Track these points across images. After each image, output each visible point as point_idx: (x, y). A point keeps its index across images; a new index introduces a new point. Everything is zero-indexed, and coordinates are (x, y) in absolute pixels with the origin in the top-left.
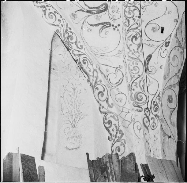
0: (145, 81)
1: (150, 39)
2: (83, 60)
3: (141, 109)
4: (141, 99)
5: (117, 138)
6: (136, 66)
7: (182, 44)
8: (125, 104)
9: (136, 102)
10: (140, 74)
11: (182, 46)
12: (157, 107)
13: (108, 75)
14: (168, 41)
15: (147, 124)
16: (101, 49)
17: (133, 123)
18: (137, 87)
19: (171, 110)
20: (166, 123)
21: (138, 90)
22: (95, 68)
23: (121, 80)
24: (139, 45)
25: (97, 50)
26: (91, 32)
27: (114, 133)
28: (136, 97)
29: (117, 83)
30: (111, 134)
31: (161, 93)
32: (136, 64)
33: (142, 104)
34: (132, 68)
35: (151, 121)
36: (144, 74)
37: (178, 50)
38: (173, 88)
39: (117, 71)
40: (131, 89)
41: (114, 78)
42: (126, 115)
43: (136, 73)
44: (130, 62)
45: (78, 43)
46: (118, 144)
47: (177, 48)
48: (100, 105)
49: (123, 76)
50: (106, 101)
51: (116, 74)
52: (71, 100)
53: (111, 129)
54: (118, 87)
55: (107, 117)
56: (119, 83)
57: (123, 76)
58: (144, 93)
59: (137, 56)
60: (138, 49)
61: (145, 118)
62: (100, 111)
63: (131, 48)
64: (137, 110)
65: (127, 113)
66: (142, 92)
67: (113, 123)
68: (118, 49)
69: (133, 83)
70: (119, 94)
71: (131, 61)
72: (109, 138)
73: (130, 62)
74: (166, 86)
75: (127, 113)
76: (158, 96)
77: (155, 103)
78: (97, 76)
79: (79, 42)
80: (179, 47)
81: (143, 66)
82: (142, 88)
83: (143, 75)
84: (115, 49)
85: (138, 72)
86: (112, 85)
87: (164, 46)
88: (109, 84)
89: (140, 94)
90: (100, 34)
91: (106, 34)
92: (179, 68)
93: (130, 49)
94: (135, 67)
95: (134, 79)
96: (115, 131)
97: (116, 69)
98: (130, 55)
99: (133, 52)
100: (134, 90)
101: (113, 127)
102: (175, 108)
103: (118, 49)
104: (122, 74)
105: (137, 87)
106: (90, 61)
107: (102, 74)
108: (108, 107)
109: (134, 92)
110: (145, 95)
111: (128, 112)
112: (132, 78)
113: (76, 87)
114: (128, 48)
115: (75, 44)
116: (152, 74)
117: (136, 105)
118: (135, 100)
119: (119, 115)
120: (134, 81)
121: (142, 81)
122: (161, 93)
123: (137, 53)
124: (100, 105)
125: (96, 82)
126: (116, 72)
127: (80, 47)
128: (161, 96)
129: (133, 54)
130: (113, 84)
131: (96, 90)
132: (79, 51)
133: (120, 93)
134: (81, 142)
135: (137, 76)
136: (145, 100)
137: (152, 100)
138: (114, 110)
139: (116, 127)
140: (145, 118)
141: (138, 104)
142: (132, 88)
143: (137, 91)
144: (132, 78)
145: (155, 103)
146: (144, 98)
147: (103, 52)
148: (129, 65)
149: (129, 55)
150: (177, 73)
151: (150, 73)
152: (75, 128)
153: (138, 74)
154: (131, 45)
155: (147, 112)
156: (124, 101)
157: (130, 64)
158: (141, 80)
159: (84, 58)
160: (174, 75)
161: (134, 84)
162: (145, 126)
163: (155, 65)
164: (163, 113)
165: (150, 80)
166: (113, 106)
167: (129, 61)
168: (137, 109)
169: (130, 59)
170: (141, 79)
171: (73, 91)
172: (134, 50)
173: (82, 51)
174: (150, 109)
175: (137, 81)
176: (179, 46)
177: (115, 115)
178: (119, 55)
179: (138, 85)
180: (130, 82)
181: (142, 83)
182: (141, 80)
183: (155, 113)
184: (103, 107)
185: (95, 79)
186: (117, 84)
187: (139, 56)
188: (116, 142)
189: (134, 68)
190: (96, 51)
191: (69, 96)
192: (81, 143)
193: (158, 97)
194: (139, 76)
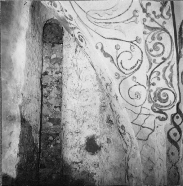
0: (173, 68)
3: (165, 117)
6: (159, 43)
9: (157, 105)
10: (165, 55)
13: (119, 56)
16: (106, 12)
18: (159, 79)
21: (161, 84)
23: (139, 63)
28: (157, 96)
29: (132, 68)
32: (158, 39)
33: (167, 108)
34: (150, 46)
36: (172, 55)
39: (132, 48)
40: (150, 82)
41: (128, 60)
42: (147, 118)
43: (159, 55)
49: (142, 56)
51: (131, 53)
54: (135, 75)
56: (136, 68)
57: (142, 56)
58: (172, 89)
59: (161, 24)
60: (161, 10)
63: (150, 10)
65: (148, 115)
68: (132, 9)
69: (152, 72)
70: (136, 85)
75: (148, 115)
81: (172, 41)
82: (169, 80)
84: (128, 10)
85: (163, 53)
88: (120, 70)
89: (164, 91)
93: (148, 12)
94: (156, 44)
95: (154, 65)
97: (132, 44)
98: (148, 23)
100: (154, 84)
103: (132, 9)
104: (141, 53)
105: (159, 79)
109: (153, 88)
110: (173, 93)
112: (151, 65)
114: (144, 11)
117: (157, 110)
118: (156, 101)
120: (155, 69)
123: (160, 18)
126: (131, 49)
129: (152, 20)
130: (127, 70)
133: (138, 84)
135: (159, 60)
136: (173, 100)
141: (160, 108)
142: (152, 82)
143: (158, 87)
144: (151, 65)
148: (146, 41)
149: (146, 23)
153: (162, 56)
157: (148, 40)
158: (167, 67)
161: (154, 75)
167: (146, 34)
168: (158, 116)
169: (148, 31)
170: (167, 65)
172: (154, 12)
175: (160, 69)
178: (134, 18)
180: (147, 72)
181: (168, 73)
182: (167, 67)
186: (133, 70)
187: (164, 23)
189: (155, 47)
190: (98, 17)
194: (164, 59)
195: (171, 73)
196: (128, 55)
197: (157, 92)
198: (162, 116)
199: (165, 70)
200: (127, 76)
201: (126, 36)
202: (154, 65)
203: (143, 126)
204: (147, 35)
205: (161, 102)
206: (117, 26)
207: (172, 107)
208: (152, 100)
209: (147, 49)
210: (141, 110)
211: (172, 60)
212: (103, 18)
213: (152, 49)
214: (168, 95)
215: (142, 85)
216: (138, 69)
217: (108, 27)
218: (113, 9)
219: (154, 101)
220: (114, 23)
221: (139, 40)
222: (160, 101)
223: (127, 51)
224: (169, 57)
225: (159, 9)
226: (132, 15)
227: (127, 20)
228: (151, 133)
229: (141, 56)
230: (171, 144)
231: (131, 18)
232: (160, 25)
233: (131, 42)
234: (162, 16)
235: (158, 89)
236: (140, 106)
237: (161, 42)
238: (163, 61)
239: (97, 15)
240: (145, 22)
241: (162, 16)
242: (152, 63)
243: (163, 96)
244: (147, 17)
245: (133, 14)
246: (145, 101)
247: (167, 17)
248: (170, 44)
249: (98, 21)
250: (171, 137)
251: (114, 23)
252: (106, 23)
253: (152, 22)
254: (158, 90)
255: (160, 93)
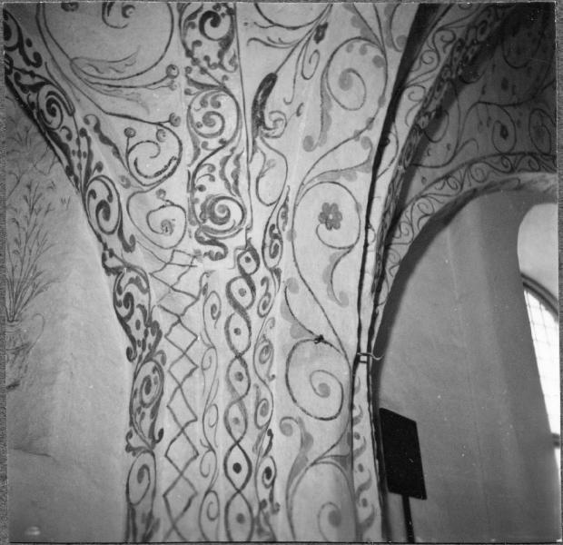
0: (240, 160)
1: (270, 21)
2: (50, 102)
3: (222, 251)
4: (226, 217)
5: (147, 351)
6: (214, 113)
7: (377, 31)
8: (180, 241)
9: (206, 229)
10: (226, 136)
11: (379, 37)
12: (279, 244)
14: (322, 23)
15: (244, 301)
16: (112, 65)
17: (202, 297)
18: (212, 179)
19: (332, 251)
20: (309, 293)
21: (218, 188)
22: (81, 124)
23: (174, 163)
24: (226, 42)
25: (97, 70)
26: (73, 10)
27: (139, 335)
28: (208, 210)
29: (158, 174)
30: (132, 339)
31: (290, 196)
32: (213, 105)
33: (227, 234)
34: (198, 118)
35: (260, 290)
36: (238, 135)
37: (363, 51)
38: (342, 180)
39: (161, 135)
40: (194, 185)
44: (193, 99)
45: (26, 46)
46: (147, 369)
47: (358, 45)
48: (105, 246)
50: (116, 232)
52: (17, 236)
53: (132, 323)
54: (162, 186)
55: (123, 284)
56: (166, 173)
58: (237, 198)
59: (220, 79)
60: (220, 55)
61: (234, 279)
62: (105, 266)
64: (208, 254)
65: (187, 268)
66: (228, 195)
67: (136, 303)
69: (199, 166)
70: (163, 207)
71: (198, 94)
72: (129, 352)
73: (193, 99)
74: (314, 173)
76: (285, 205)
77: (276, 231)
78: (90, 152)
79: (30, 44)
80: (363, 42)
82: (231, 181)
83: (237, 139)
84: (156, 64)
85: (221, 130)
86: (141, 178)
87: (313, 42)
88: (131, 174)
89: (222, 202)
90: (106, 15)
91: (125, 16)
92: (372, 115)
93: (195, 56)
95: (204, 153)
96: (143, 327)
97: (160, 128)
98: (195, 75)
99: (204, 64)
100: (201, 188)
101: (138, 314)
102: (351, 248)
103: (165, 62)
105: (212, 179)
106: (66, 102)
107: (105, 143)
108: (123, 252)
109: (201, 196)
110: (240, 206)
111: (191, 266)
112: (197, 152)
113: (38, 193)
114: (189, 53)
115: (17, 50)
116: (275, 137)
117: (207, 239)
118: (204, 221)
119: (151, 274)
121: (231, 161)
122: (292, 197)
124: (105, 246)
125: (88, 173)
127: (33, 60)
128: (290, 205)
129: (203, 71)
130: (146, 177)
131: (91, 199)
132: (32, 74)
133: (168, 203)
134: (26, 366)
135: (214, 143)
137: (268, 223)
138: (138, 257)
139: (145, 313)
140: (234, 279)
141: (212, 235)
142: (198, 184)
144: (197, 152)
145: (276, 231)
146: (236, 214)
147: (118, 76)
148: (190, 107)
150: (361, 132)
151: (267, 136)
152: (15, 323)
153: (219, 138)
154: (197, 43)
155: (248, 260)
156: (178, 231)
157: (193, 106)
158: (228, 157)
159: (50, 97)
160: (351, 135)
161: (204, 170)
162: (236, 305)
163: (285, 109)
164: (295, 260)
165: (268, 158)
166: (134, 244)
168: (207, 251)
169: (194, 90)
170: (228, 153)
171: (25, 207)
172: (207, 58)
173: (40, 71)
174: (259, 252)
176: (365, 39)
177: (141, 275)
178: (169, 80)
179: (216, 174)
180: (189, 166)
181: (230, 168)
182: (228, 157)
183: (272, 263)
184: (112, 254)
185: (84, 161)
186: (161, 177)
187: (225, 78)
188: (145, 362)
189: (207, 120)
190: (95, 73)
191: (15, 224)
192: (25, 371)
193: (283, 210)
194: (224, 143)
195: (235, 167)
196: (152, 149)
197: (208, 204)
198: (215, 252)
199: (224, 162)
200: (145, 188)
201: (148, 112)
202: (204, 153)
203: (176, 287)
204: (193, 97)
205: (215, 223)
206: (133, 93)
207: (237, 233)
208: (196, 217)
209: (192, 122)
210: (172, 256)
211: (238, 144)
212: (105, 75)
213: (202, 122)
214: (228, 210)
215: (178, 206)
216: (170, 174)
217: (113, 93)
218: (127, 62)
219: (201, 221)
220: (126, 87)
221: (176, 120)
222: (213, 221)
223: (148, 141)
224: (232, 140)
225: (216, 53)
226: (165, 75)
227: (155, 83)
228: (193, 304)
229: (177, 151)
230: (233, 311)
231: (162, 80)
232: (218, 82)
233: (159, 124)
234: (221, 65)
235: (210, 198)
236: (171, 248)
237: (218, 110)
238: (221, 145)
239: (93, 68)
240: (190, 73)
241: (221, 65)
242: (199, 150)
243: (220, 212)
244: (194, 65)
245: (167, 70)
246: (183, 237)
247: (230, 68)
248: (235, 117)
249: (94, 80)
250: (234, 295)
251: (126, 87)
252: (110, 86)
253: (202, 74)
254: (210, 201)
255: (212, 205)
